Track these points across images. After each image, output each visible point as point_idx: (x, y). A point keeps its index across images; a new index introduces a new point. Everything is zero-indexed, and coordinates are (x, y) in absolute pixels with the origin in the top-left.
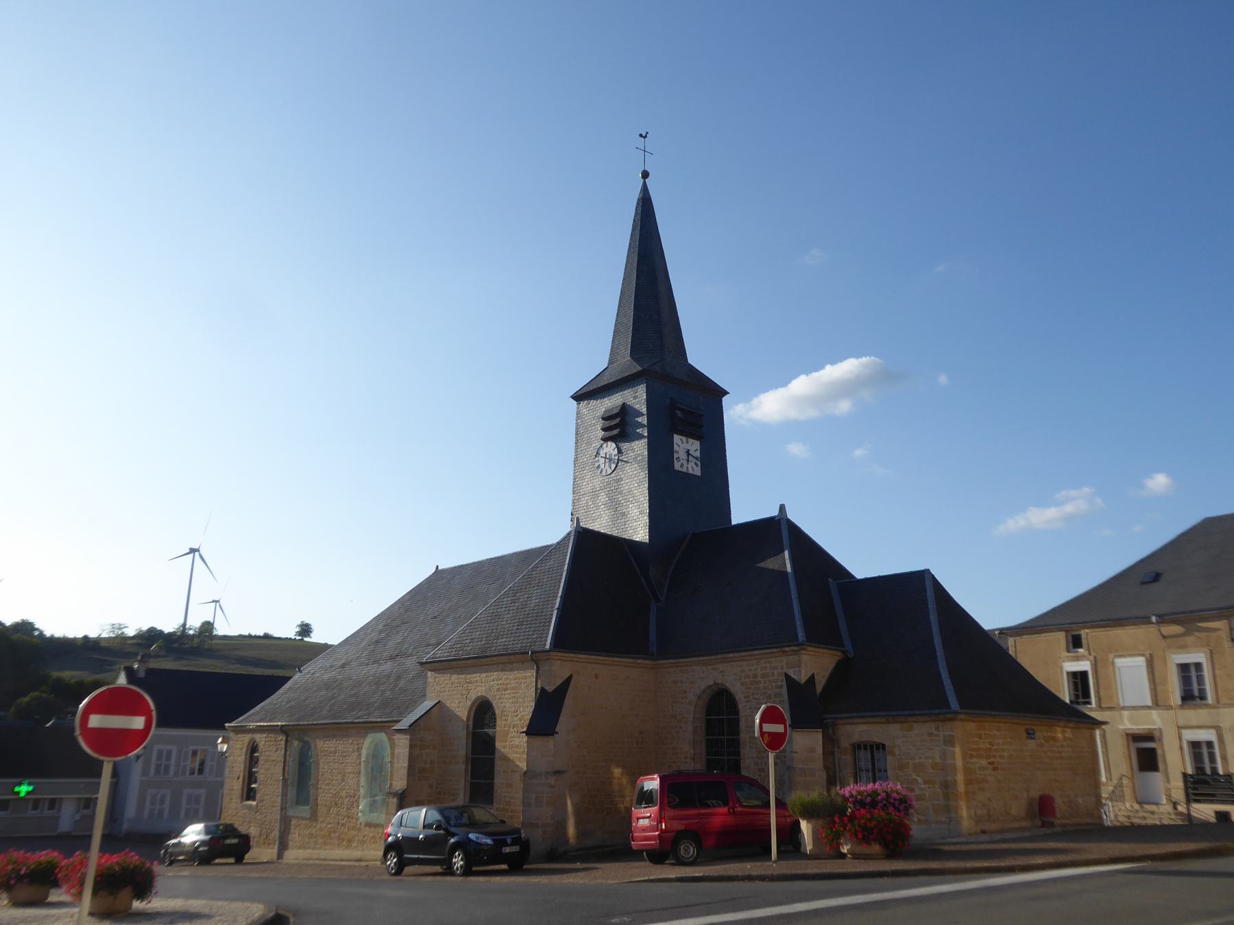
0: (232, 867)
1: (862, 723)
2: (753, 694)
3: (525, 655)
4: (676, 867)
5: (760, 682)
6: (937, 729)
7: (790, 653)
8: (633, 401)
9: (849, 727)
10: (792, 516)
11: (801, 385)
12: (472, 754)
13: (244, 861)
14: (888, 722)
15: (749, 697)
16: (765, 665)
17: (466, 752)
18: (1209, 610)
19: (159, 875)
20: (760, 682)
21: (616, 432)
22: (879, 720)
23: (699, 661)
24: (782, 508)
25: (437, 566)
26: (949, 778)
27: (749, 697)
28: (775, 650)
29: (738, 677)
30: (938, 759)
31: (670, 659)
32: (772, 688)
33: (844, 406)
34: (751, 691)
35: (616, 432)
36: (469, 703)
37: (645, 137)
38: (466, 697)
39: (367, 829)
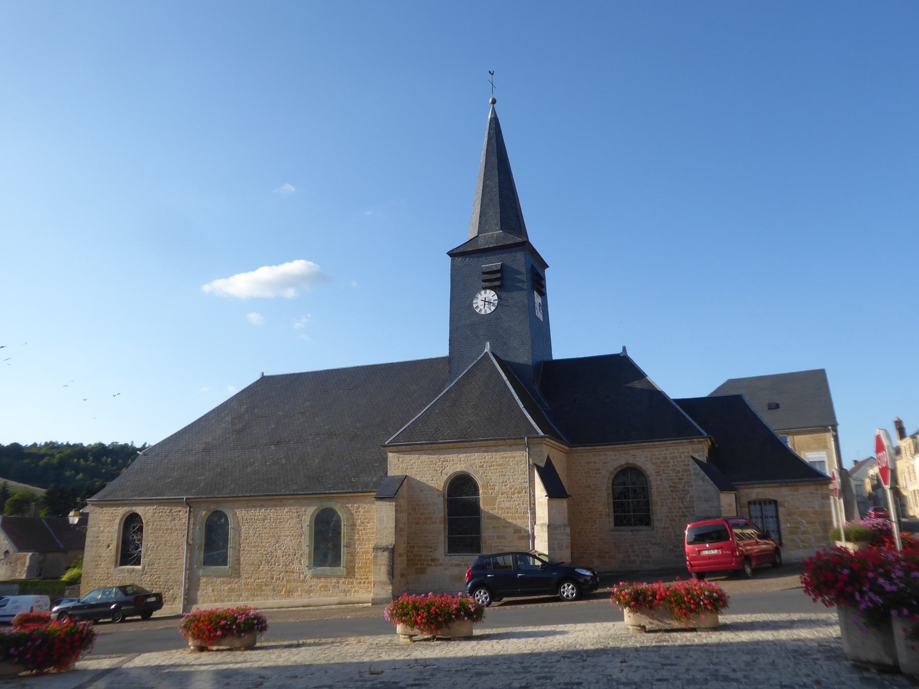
0: (140, 623)
1: (760, 487)
2: (663, 470)
3: (522, 440)
4: (727, 582)
5: (669, 462)
6: (816, 490)
7: (696, 443)
8: (512, 263)
9: (746, 491)
10: (631, 355)
11: (265, 273)
12: (448, 516)
13: (152, 617)
14: (781, 486)
15: (660, 472)
16: (674, 451)
17: (444, 514)
18: (803, 428)
19: (98, 635)
20: (669, 462)
21: (497, 283)
22: (776, 485)
23: (614, 448)
24: (624, 348)
25: (263, 373)
26: (827, 520)
27: (660, 472)
28: (684, 441)
29: (649, 459)
30: (817, 508)
31: (587, 446)
32: (681, 466)
33: (290, 293)
34: (662, 468)
35: (497, 283)
36: (445, 477)
37: (492, 74)
38: (441, 472)
39: (315, 580)
